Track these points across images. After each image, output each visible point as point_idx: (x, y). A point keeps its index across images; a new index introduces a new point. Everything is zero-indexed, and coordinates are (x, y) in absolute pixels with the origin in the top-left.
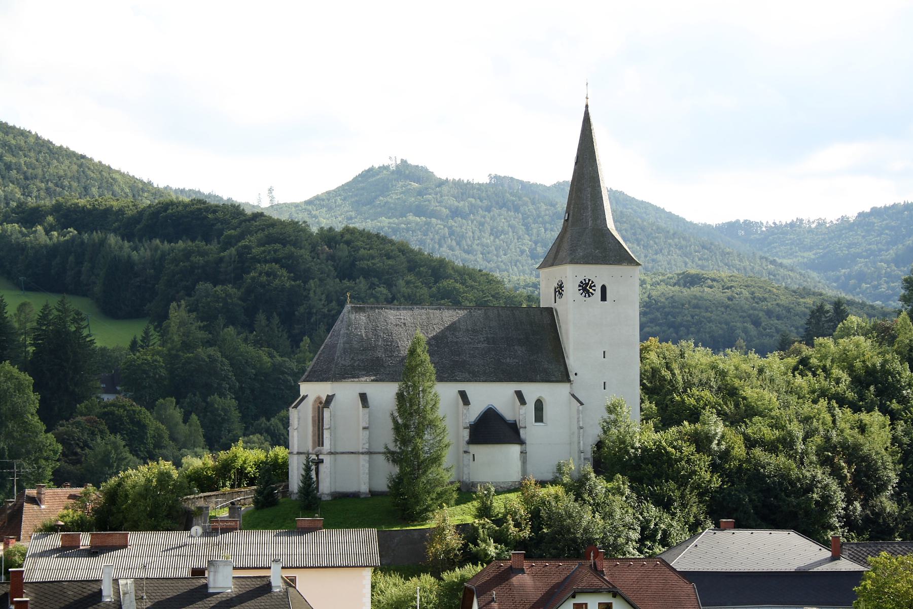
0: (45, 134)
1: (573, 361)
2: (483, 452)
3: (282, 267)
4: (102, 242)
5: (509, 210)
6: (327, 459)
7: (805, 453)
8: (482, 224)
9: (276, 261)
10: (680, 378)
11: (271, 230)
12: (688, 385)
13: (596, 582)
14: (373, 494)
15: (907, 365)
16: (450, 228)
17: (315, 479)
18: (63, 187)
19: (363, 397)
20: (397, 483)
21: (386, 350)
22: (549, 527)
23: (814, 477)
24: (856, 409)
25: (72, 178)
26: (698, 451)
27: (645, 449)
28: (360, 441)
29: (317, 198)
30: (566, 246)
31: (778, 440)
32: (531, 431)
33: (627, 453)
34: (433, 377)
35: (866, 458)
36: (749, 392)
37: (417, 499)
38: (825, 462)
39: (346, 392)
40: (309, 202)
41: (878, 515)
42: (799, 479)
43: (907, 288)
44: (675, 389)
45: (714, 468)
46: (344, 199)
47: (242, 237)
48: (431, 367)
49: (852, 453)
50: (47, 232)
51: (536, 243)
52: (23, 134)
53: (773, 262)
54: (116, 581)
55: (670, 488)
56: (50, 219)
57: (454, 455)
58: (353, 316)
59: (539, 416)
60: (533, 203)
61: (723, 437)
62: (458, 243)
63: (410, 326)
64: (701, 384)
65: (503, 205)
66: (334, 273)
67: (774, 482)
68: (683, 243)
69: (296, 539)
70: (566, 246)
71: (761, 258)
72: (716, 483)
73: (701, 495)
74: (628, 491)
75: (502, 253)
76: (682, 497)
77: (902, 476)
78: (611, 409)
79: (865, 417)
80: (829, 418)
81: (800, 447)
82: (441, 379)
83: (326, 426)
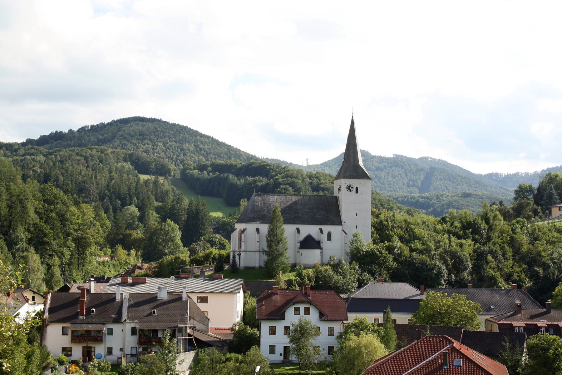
0: (216, 137)
1: (344, 217)
2: (305, 252)
3: (290, 186)
4: (227, 177)
5: (399, 167)
6: (242, 253)
7: (435, 255)
8: (388, 173)
9: (288, 184)
10: (390, 225)
11: (287, 173)
12: (393, 227)
13: (304, 299)
14: (260, 267)
15: (484, 221)
16: (376, 174)
17: (238, 263)
18: (221, 157)
19: (258, 230)
20: (267, 263)
21: (268, 211)
22: (322, 281)
23: (436, 264)
24: (459, 237)
25: (225, 154)
26: (389, 253)
27: (367, 252)
28: (256, 247)
29: (325, 163)
30: (342, 171)
31: (424, 249)
32: (325, 244)
33: (360, 253)
34: (282, 222)
35: (459, 257)
36: (416, 230)
37: (274, 270)
38: (442, 258)
39: (251, 227)
40: (322, 164)
41: (462, 280)
42: (429, 265)
43: (516, 194)
44: (388, 230)
45: (395, 260)
46: (335, 163)
47: (276, 175)
48: (282, 218)
49: (454, 255)
50: (208, 173)
51: (409, 181)
52: (208, 137)
53: (505, 189)
54: (122, 294)
55: (375, 267)
56: (210, 168)
57: (290, 252)
58: (256, 198)
59: (329, 239)
60: (409, 165)
61: (400, 247)
62: (379, 181)
63: (276, 201)
64: (399, 227)
65: (397, 166)
66: (310, 189)
67: (419, 266)
68: (468, 181)
69: (211, 282)
70: (342, 171)
71: (500, 187)
72: (395, 265)
73: (388, 270)
74: (357, 268)
75: (396, 184)
76: (380, 271)
77: (474, 265)
78: (355, 236)
79: (463, 241)
80: (447, 241)
81: (433, 252)
82: (285, 223)
83: (242, 240)
